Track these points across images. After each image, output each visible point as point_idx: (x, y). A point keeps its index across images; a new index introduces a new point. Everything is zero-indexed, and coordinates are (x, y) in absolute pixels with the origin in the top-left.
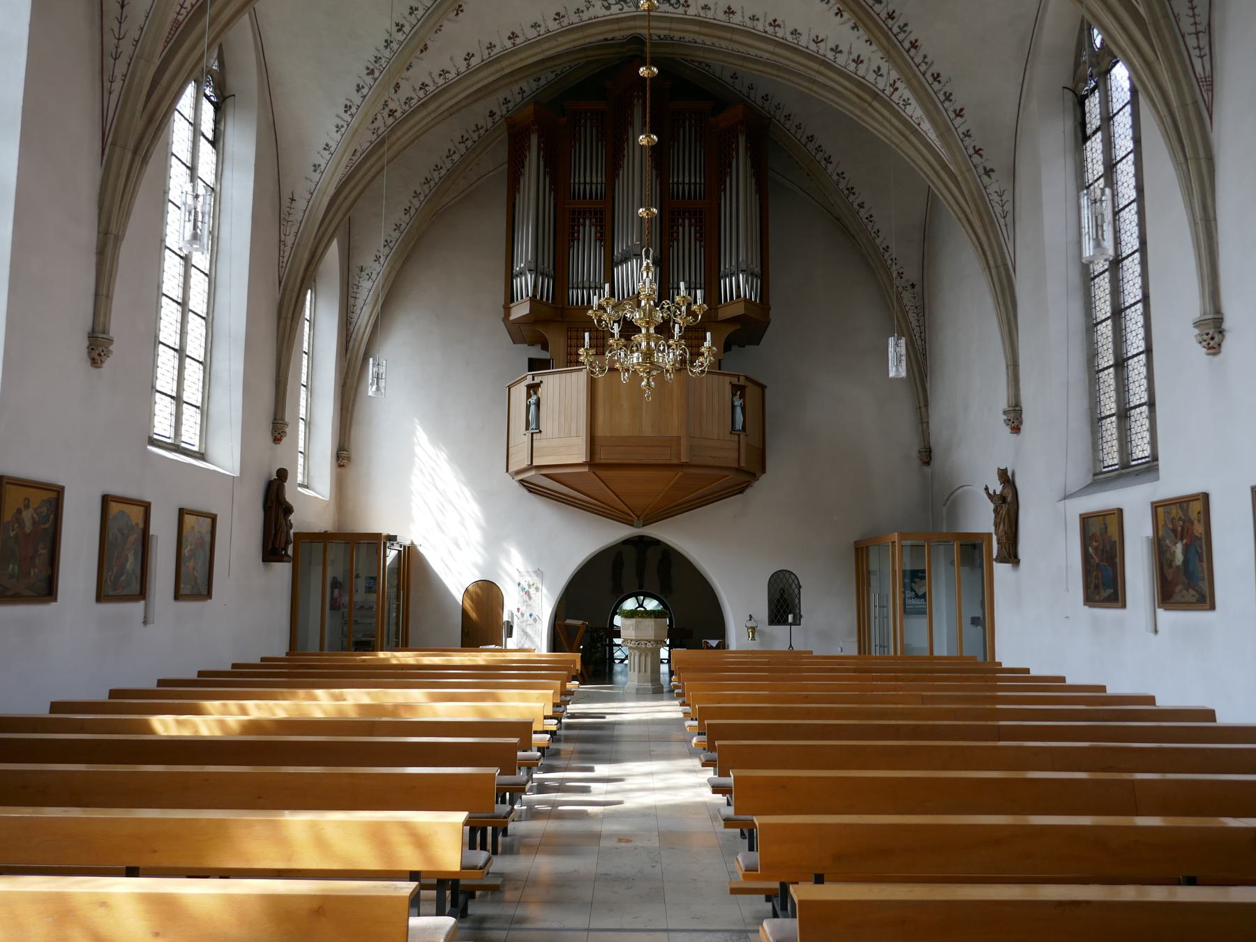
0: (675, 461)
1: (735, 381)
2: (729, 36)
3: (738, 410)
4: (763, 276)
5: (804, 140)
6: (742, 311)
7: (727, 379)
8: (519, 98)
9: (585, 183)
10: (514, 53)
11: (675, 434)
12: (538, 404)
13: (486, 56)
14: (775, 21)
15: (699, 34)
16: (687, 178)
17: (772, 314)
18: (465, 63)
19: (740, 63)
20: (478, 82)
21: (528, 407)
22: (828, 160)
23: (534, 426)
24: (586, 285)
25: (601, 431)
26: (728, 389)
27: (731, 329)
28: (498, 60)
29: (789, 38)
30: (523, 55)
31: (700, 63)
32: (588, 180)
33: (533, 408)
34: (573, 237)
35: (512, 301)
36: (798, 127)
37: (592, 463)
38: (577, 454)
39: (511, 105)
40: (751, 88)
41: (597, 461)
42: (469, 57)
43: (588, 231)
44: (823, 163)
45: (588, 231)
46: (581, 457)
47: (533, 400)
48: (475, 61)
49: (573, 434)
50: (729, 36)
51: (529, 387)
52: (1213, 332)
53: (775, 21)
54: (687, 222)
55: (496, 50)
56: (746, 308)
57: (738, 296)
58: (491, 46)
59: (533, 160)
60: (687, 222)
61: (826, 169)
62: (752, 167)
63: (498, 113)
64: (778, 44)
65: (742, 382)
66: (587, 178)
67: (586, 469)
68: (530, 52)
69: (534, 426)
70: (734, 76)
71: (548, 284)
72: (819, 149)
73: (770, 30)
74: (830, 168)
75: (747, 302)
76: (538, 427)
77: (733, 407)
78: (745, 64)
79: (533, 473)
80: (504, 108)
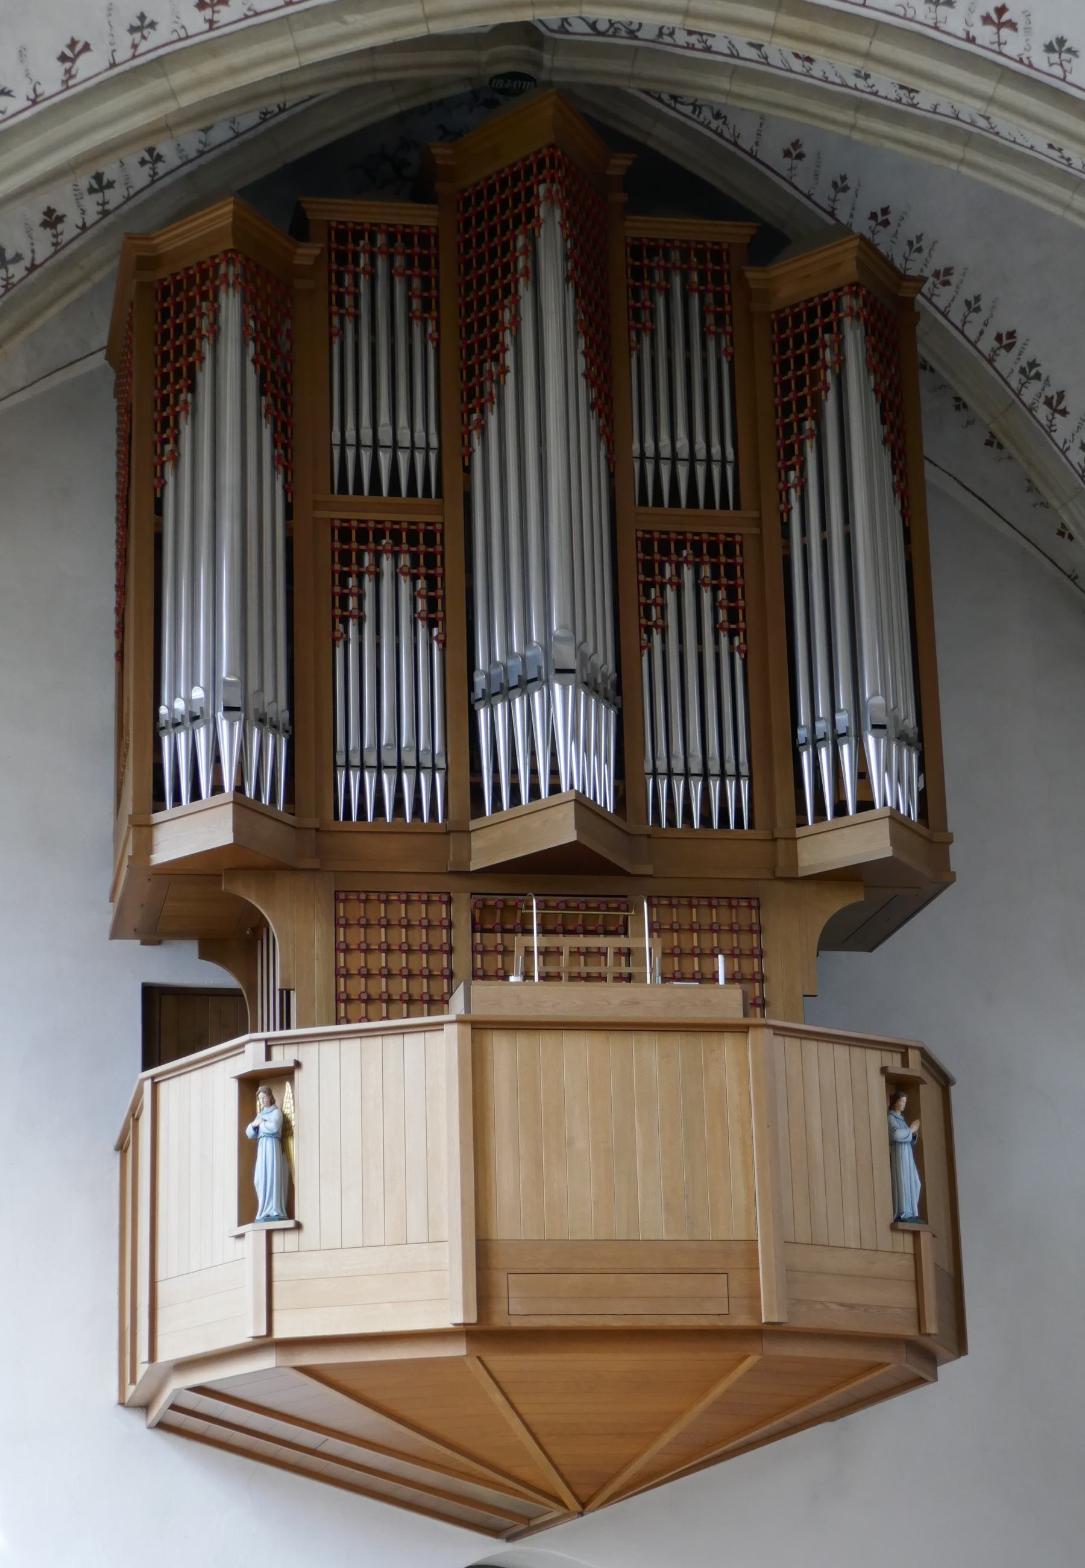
0: (742, 1320)
1: (894, 1062)
2: (862, 42)
3: (907, 1154)
4: (923, 739)
5: (987, 344)
6: (568, 835)
7: (874, 1059)
8: (140, 177)
9: (376, 446)
10: (209, 49)
11: (738, 1233)
12: (284, 1132)
13: (123, 53)
14: (1001, 10)
15: (773, 30)
16: (686, 436)
17: (956, 853)
18: (60, 69)
19: (847, 117)
20: (95, 127)
21: (247, 1150)
22: (1056, 404)
23: (269, 1201)
24: (390, 758)
25: (509, 1225)
26: (878, 1089)
27: (836, 902)
28: (159, 65)
29: (1040, 59)
30: (238, 57)
31: (696, 107)
32: (385, 437)
33: (266, 1150)
34: (343, 612)
35: (158, 801)
36: (973, 305)
37: (482, 1333)
38: (440, 1300)
39: (114, 197)
40: (840, 186)
41: (500, 1321)
42: (73, 52)
43: (390, 592)
44: (1043, 413)
45: (390, 592)
46: (447, 1306)
47: (267, 1120)
48: (88, 67)
49: (416, 1232)
50: (862, 42)
51: (249, 1084)
52: (626, 896)
53: (1001, 10)
54: (688, 574)
55: (155, 38)
56: (894, 841)
57: (555, 789)
58: (143, 25)
59: (228, 371)
60: (688, 574)
61: (1050, 429)
62: (262, 391)
63: (73, 220)
64: (1005, 75)
65: (915, 1067)
66: (386, 422)
67: (458, 1350)
68: (257, 51)
69: (269, 1201)
70: (795, 151)
71: (276, 747)
72: (1031, 371)
73: (985, 34)
74: (1063, 428)
75: (583, 805)
76: (289, 1210)
77: (894, 1144)
78: (863, 121)
79: (267, 1362)
80: (91, 205)
